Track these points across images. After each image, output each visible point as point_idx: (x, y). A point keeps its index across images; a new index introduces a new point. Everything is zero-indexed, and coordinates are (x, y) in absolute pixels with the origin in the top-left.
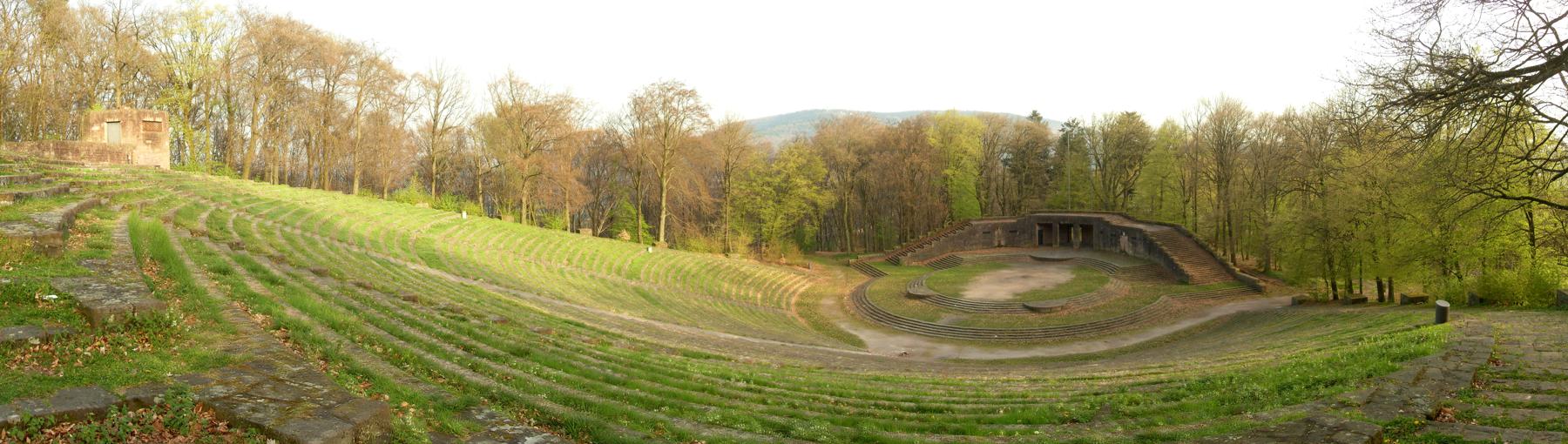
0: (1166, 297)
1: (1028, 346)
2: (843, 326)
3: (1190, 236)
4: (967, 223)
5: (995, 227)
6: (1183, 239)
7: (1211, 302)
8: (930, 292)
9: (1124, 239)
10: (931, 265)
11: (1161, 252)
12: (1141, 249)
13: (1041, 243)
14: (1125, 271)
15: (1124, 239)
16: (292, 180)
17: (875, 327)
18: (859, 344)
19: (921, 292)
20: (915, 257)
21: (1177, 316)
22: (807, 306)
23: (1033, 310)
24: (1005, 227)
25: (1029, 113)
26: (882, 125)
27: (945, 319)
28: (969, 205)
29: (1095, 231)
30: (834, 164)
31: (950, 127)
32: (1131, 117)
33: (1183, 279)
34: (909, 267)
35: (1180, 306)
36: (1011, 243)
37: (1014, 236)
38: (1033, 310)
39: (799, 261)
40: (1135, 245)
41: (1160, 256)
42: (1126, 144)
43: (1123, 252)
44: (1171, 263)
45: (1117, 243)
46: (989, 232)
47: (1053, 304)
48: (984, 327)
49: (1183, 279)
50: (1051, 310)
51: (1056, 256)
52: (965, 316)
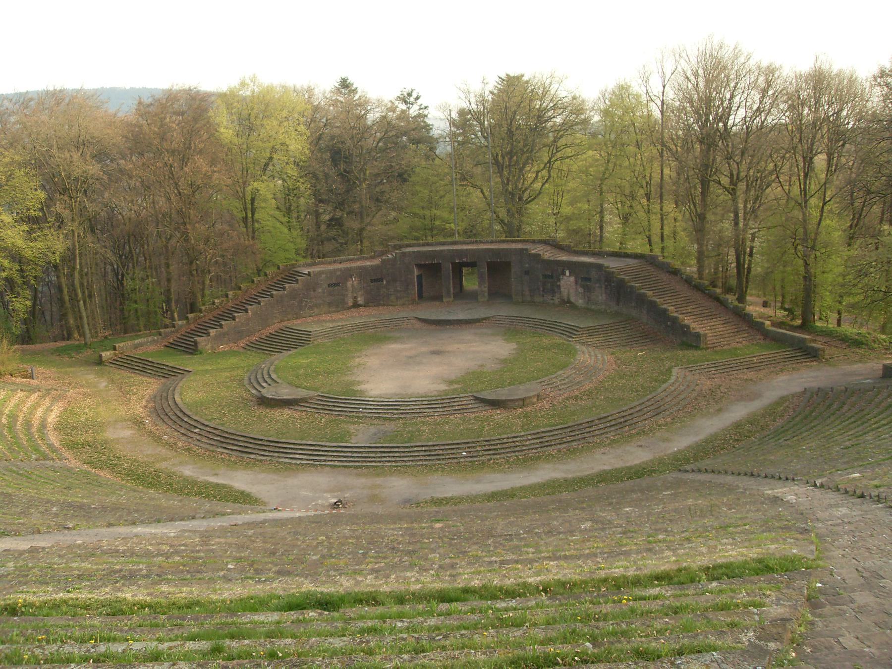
0: (681, 374)
1: (527, 462)
2: (188, 471)
3: (675, 272)
4: (291, 275)
5: (347, 274)
6: (664, 277)
7: (750, 375)
8: (301, 393)
9: (567, 282)
10: (253, 347)
11: (641, 300)
12: (600, 296)
13: (420, 296)
14: (591, 332)
15: (567, 282)
16: (56, 606)
17: (247, 466)
18: (244, 499)
19: (285, 393)
20: (219, 338)
21: (715, 399)
22: (80, 439)
23: (495, 404)
24: (363, 273)
25: (335, 82)
26: (126, 111)
27: (361, 434)
28: (281, 237)
29: (515, 270)
30: (58, 185)
31: (252, 112)
32: (511, 84)
33: (690, 341)
34: (216, 355)
35: (707, 384)
36: (374, 300)
37: (378, 287)
38: (495, 404)
39: (13, 366)
40: (588, 289)
41: (637, 303)
42: (515, 130)
43: (567, 303)
44: (661, 315)
45: (554, 289)
46: (337, 283)
47: (520, 392)
48: (410, 439)
49: (690, 341)
50: (523, 402)
51: (461, 316)
52: (389, 427)
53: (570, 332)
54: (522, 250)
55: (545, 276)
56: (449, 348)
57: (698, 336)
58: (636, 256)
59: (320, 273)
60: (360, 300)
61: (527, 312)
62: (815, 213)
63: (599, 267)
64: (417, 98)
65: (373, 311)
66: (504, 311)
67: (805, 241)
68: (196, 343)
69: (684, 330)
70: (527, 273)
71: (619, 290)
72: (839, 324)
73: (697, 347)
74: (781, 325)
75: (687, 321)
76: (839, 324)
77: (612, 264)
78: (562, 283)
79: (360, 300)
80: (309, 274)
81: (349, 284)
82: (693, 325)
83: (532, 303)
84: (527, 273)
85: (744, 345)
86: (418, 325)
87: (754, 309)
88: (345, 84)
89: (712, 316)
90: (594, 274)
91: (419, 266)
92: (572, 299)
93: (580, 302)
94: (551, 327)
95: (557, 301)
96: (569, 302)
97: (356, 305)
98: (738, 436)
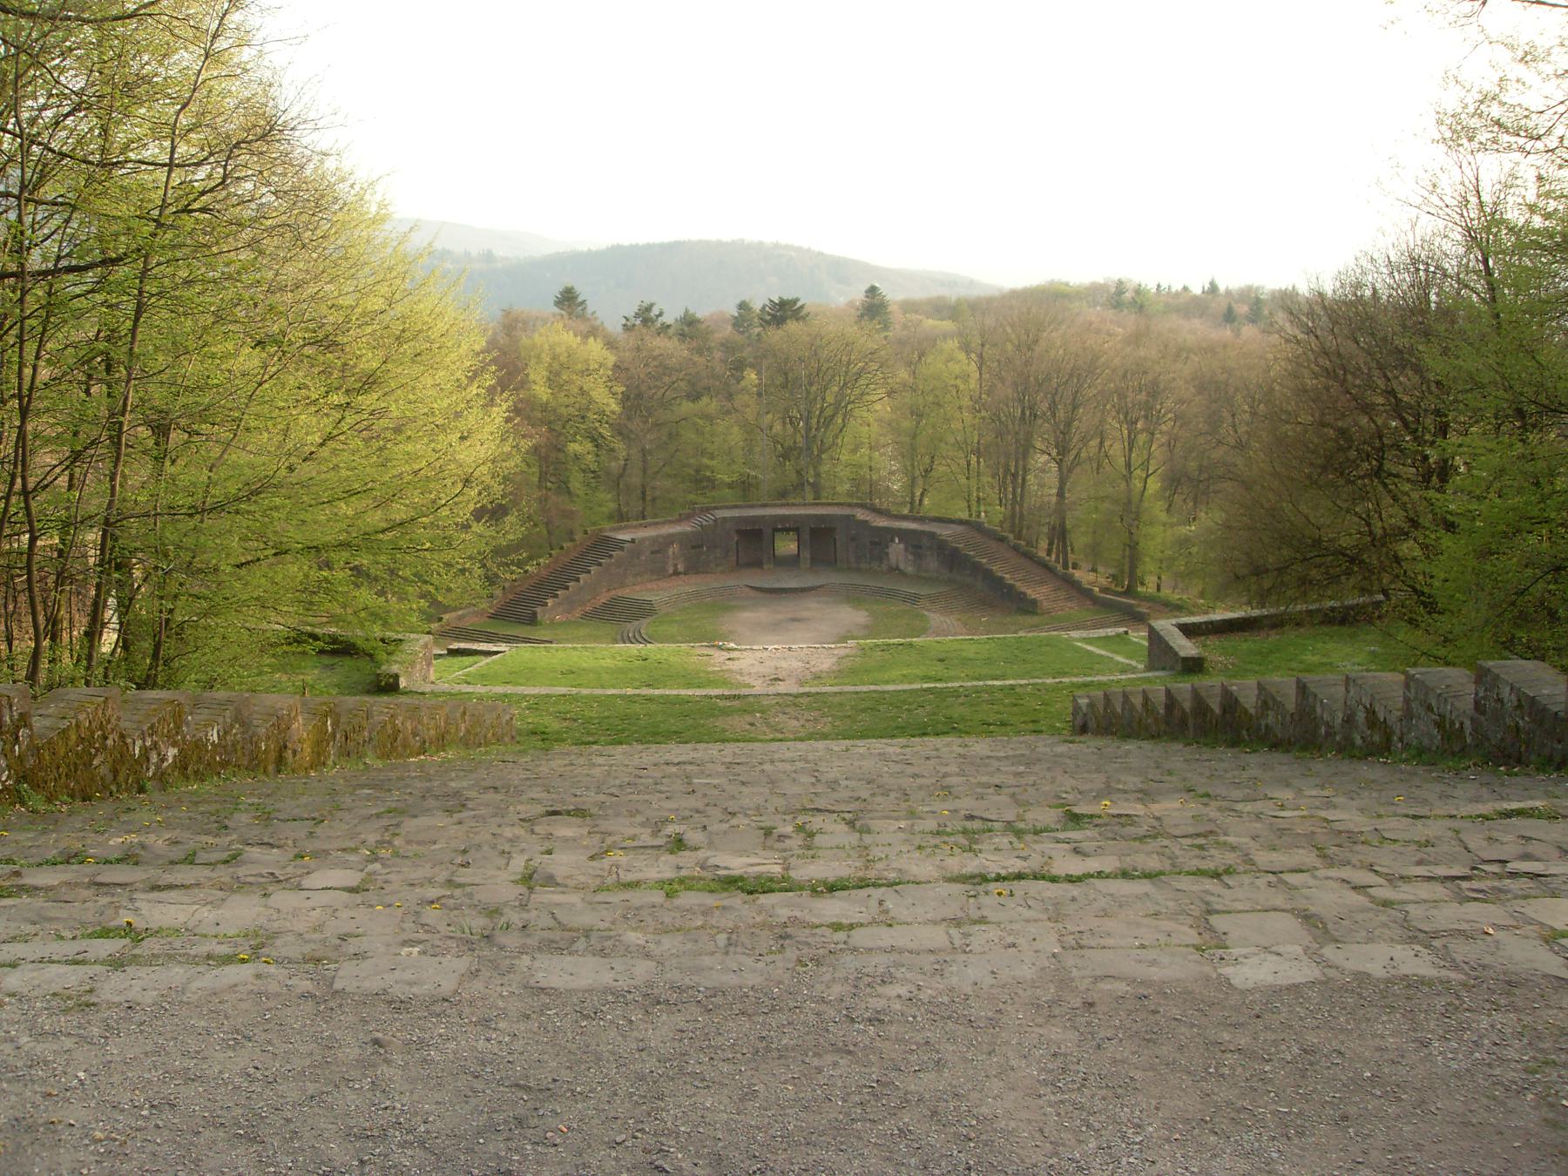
5: (669, 540)
9: (897, 549)
11: (976, 568)
12: (932, 563)
15: (897, 549)
24: (682, 538)
33: (1027, 607)
36: (694, 568)
37: (699, 554)
43: (895, 570)
45: (881, 556)
49: (1027, 607)
51: (793, 584)
53: (914, 599)
54: (848, 517)
55: (872, 543)
56: (806, 614)
57: (1034, 602)
58: (961, 522)
59: (643, 540)
60: (681, 568)
61: (857, 579)
62: (1139, 485)
63: (932, 535)
64: (661, 314)
65: (694, 579)
66: (835, 579)
67: (1130, 511)
68: (535, 614)
69: (1021, 597)
70: (853, 539)
71: (952, 558)
72: (1159, 589)
73: (1033, 613)
74: (1105, 590)
75: (1021, 587)
76: (1159, 589)
77: (944, 532)
78: (890, 550)
79: (681, 568)
80: (633, 541)
81: (670, 551)
82: (1029, 592)
83: (858, 570)
84: (853, 539)
85: (1072, 609)
86: (752, 593)
87: (1082, 576)
88: (872, 290)
89: (1042, 583)
90: (925, 541)
91: (739, 532)
92: (902, 566)
93: (910, 569)
94: (890, 595)
95: (884, 567)
96: (897, 568)
97: (676, 573)
98: (710, 683)
